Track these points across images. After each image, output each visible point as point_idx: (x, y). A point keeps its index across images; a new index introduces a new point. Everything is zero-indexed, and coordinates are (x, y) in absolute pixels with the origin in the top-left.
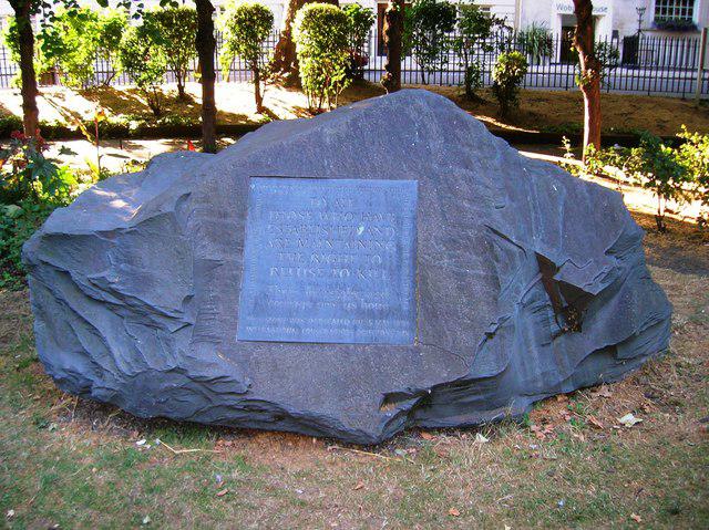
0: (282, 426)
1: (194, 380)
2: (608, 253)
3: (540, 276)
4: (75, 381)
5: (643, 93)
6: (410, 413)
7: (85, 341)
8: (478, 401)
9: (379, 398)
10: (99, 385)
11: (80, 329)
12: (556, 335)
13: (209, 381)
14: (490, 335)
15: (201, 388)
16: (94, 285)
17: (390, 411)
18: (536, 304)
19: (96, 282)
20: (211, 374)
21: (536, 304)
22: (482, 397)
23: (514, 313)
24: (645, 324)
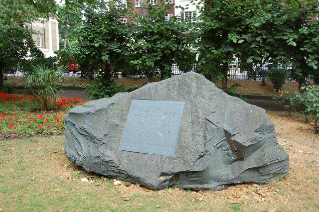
0: (129, 179)
1: (103, 161)
2: (255, 131)
6: (170, 180)
7: (77, 146)
9: (160, 174)
12: (233, 161)
14: (201, 157)
17: (163, 178)
20: (108, 159)
22: (197, 179)
23: (211, 148)
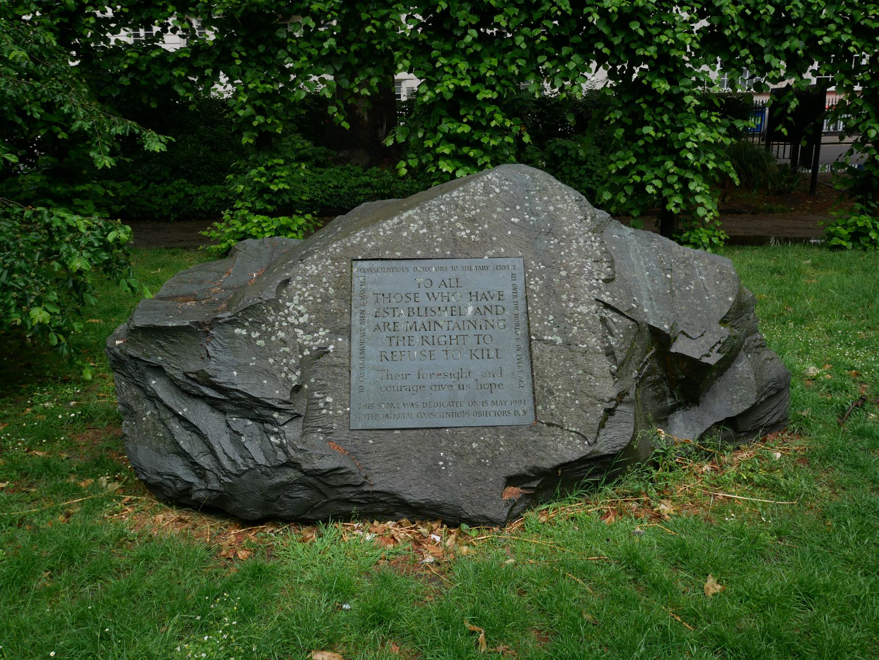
1: (307, 473)
4: (171, 484)
5: (785, 160)
9: (501, 483)
15: (316, 482)
16: (193, 380)
19: (192, 376)
20: (326, 464)
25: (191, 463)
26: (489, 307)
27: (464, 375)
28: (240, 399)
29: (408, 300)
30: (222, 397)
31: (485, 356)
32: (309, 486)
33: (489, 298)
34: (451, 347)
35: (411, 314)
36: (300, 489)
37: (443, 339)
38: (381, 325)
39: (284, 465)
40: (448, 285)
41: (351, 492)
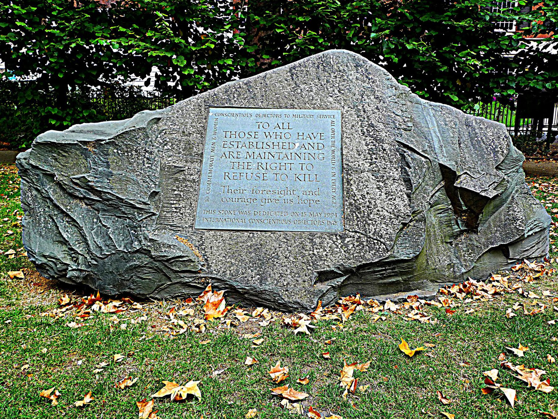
3: (443, 183)
4: (53, 265)
8: (398, 282)
10: (74, 267)
11: (62, 224)
13: (168, 260)
15: (162, 267)
16: (76, 184)
18: (440, 206)
19: (78, 181)
21: (440, 206)
24: (531, 229)
25: (69, 249)
26: (312, 144)
27: (289, 192)
28: (111, 200)
29: (250, 136)
30: (98, 198)
31: (307, 179)
32: (158, 270)
33: (313, 138)
34: (280, 172)
35: (251, 146)
36: (150, 272)
37: (274, 165)
38: (227, 154)
39: (137, 251)
40: (281, 127)
41: (191, 277)
